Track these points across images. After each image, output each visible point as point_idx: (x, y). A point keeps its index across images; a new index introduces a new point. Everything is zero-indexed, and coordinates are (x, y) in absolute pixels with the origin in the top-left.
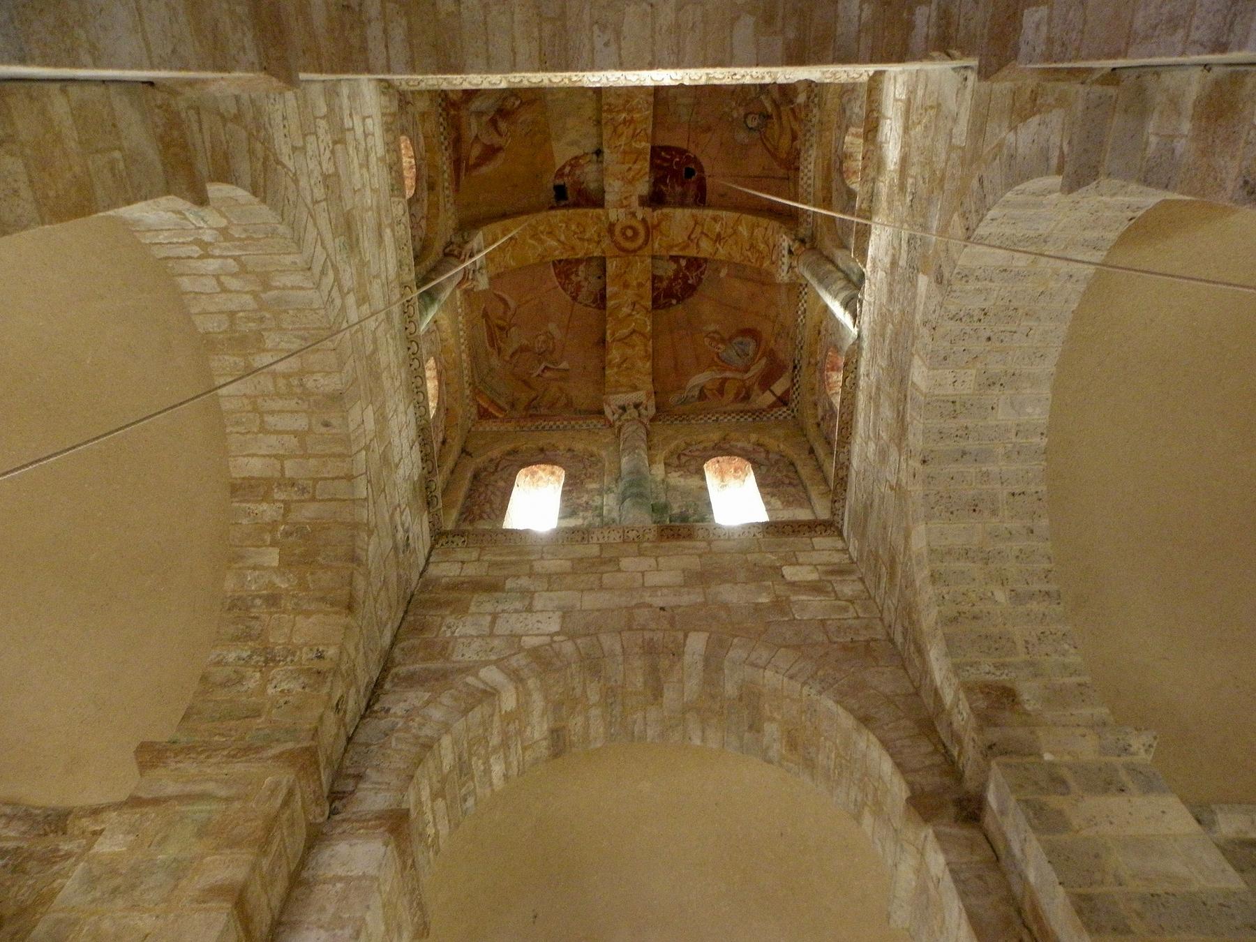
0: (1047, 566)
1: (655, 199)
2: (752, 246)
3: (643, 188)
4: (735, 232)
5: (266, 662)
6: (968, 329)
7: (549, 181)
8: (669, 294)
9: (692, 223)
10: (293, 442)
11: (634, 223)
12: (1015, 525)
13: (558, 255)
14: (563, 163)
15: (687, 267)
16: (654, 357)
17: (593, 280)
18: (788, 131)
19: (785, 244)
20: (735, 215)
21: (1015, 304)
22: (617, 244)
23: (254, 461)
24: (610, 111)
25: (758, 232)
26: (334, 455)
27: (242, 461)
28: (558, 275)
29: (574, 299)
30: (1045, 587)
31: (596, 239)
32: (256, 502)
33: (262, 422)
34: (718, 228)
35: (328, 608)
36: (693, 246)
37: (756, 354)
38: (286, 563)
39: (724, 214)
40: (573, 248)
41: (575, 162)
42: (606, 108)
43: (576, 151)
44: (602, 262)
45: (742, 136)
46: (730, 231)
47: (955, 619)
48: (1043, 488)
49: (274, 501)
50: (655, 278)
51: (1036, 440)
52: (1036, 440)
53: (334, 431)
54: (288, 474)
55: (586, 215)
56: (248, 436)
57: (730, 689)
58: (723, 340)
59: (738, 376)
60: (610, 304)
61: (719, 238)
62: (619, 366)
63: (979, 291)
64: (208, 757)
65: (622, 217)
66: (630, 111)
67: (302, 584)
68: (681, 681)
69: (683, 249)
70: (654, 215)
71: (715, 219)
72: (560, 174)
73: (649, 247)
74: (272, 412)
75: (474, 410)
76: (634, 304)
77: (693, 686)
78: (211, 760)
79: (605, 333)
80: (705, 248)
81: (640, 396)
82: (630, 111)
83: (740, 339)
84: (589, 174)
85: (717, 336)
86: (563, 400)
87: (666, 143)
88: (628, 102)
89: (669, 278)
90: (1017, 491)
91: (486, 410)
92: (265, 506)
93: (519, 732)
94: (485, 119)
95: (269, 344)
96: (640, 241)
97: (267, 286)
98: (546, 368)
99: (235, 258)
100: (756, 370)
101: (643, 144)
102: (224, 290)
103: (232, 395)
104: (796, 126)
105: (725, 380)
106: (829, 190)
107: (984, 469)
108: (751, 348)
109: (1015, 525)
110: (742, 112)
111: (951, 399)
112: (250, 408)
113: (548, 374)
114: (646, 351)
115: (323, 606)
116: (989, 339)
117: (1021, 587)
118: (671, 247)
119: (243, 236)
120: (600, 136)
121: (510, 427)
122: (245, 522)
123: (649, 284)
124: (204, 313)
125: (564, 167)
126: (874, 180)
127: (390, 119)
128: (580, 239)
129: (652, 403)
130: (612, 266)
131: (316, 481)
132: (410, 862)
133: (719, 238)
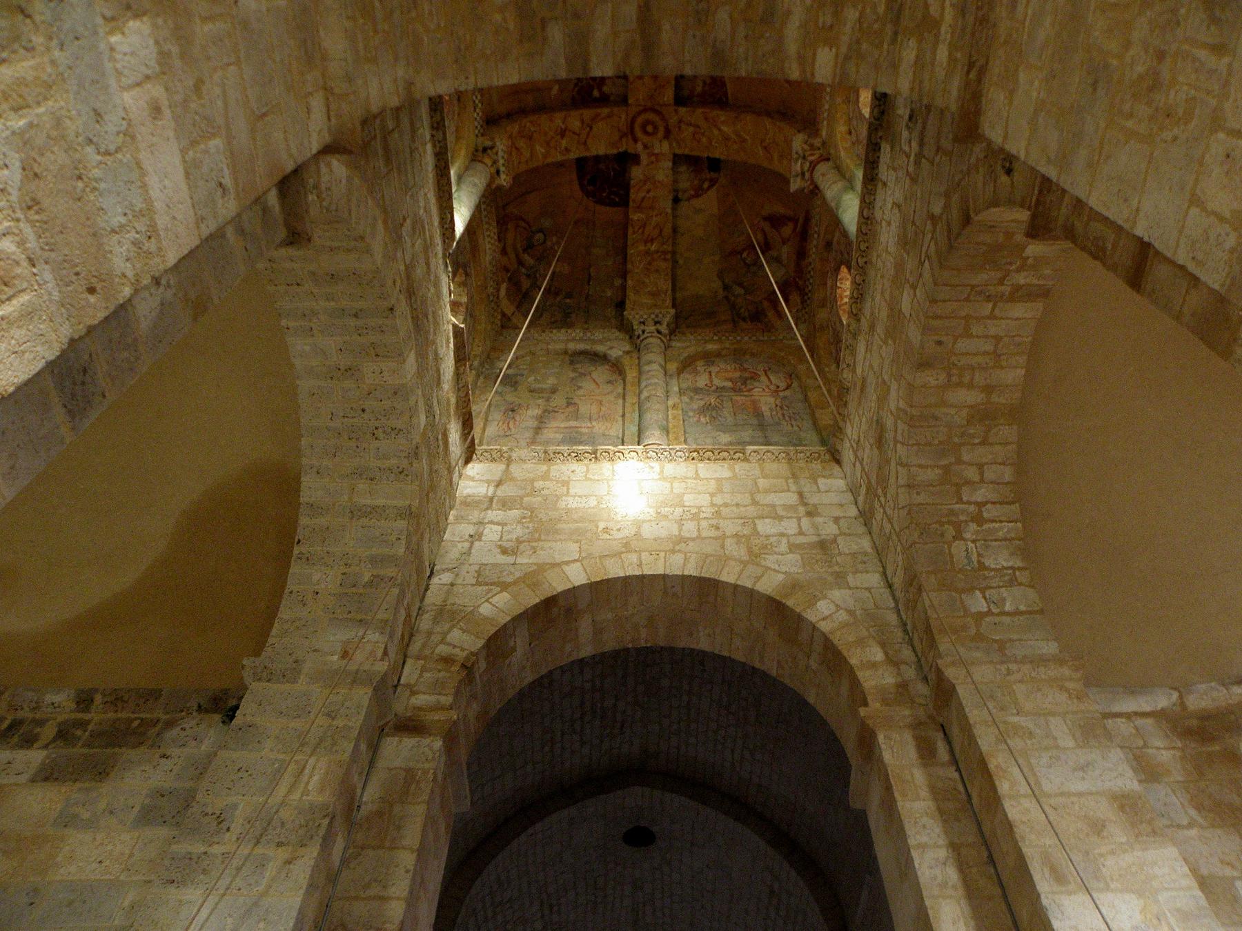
1: (626, 160)
2: (531, 138)
3: (636, 173)
4: (548, 144)
9: (589, 141)
10: (975, 330)
11: (645, 139)
13: (722, 115)
14: (709, 193)
19: (503, 176)
21: (353, 444)
22: (663, 119)
23: (1017, 315)
24: (664, 253)
25: (527, 154)
26: (940, 317)
31: (683, 126)
33: (996, 345)
34: (564, 143)
39: (560, 158)
40: (706, 119)
41: (698, 192)
42: (669, 256)
43: (695, 202)
45: (547, 223)
46: (552, 144)
48: (271, 289)
51: (291, 324)
54: (991, 305)
57: (556, 34)
65: (657, 145)
66: (647, 253)
69: (597, 115)
70: (626, 146)
71: (567, 150)
72: (713, 182)
74: (986, 353)
82: (647, 253)
87: (615, 209)
88: (650, 263)
92: (1022, 282)
95: (964, 412)
96: (640, 120)
97: (946, 469)
99: (960, 501)
102: (980, 466)
103: (1013, 375)
107: (332, 303)
110: (549, 243)
116: (363, 410)
118: (609, 116)
120: (675, 217)
122: (1047, 272)
125: (709, 188)
128: (699, 127)
131: (967, 300)
132: (972, 75)
133: (563, 134)
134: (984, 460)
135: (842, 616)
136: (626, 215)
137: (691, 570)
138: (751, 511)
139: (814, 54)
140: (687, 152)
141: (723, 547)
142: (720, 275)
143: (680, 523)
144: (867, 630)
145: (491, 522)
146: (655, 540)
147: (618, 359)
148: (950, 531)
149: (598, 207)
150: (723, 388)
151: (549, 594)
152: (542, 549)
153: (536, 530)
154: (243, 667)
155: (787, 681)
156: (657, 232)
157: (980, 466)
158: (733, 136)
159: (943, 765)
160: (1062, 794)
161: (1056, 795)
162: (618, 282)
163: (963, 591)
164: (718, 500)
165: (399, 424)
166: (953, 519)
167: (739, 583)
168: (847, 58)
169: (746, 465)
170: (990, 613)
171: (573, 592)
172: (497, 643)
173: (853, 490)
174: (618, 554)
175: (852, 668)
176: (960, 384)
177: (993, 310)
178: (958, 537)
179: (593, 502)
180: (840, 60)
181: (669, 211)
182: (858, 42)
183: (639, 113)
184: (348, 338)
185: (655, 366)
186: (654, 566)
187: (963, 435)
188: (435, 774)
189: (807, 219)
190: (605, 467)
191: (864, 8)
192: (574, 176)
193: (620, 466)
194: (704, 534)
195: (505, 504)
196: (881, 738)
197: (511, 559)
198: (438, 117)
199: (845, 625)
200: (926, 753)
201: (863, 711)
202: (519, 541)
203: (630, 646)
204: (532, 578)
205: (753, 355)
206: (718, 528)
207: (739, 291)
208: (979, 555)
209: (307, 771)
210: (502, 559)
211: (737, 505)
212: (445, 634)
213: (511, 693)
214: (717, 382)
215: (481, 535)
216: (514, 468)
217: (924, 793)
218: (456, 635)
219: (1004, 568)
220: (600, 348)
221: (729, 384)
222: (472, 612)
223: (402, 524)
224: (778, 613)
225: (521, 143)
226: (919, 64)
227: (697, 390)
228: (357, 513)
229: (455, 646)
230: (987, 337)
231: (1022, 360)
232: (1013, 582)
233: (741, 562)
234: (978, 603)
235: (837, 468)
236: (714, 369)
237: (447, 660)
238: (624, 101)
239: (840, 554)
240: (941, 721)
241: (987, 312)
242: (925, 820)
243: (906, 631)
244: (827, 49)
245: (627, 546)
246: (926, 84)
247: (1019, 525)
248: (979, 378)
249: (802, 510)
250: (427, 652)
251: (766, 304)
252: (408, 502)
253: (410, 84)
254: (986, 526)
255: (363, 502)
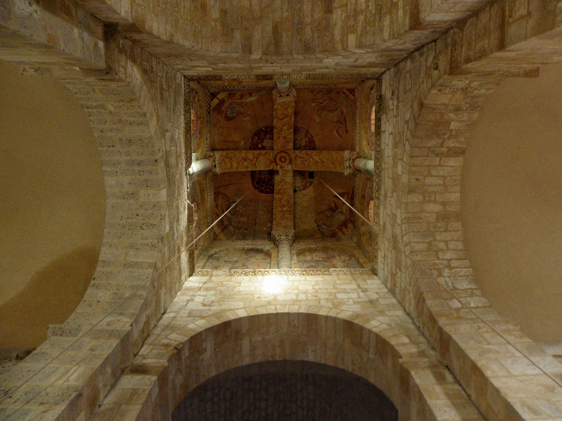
0: (91, 118)
1: (272, 173)
2: (231, 159)
3: (277, 178)
5: (467, 89)
6: (147, 220)
7: (315, 181)
8: (266, 132)
10: (434, 172)
12: (110, 134)
13: (314, 153)
15: (258, 144)
16: (272, 109)
17: (299, 139)
18: (219, 207)
19: (217, 169)
20: (238, 170)
21: (130, 232)
22: (289, 156)
24: (291, 211)
27: (457, 164)
28: (314, 141)
29: (307, 131)
30: (90, 110)
31: (297, 158)
32: (456, 147)
33: (444, 181)
34: (246, 164)
35: (432, 106)
36: (256, 155)
37: (227, 111)
38: (448, 123)
40: (307, 155)
42: (292, 213)
43: (303, 192)
44: (295, 148)
47: (131, 100)
48: (100, 149)
49: (447, 147)
50: (272, 139)
51: (108, 169)
52: (108, 169)
53: (415, 177)
54: (438, 159)
55: (301, 168)
56: (451, 175)
57: (238, 35)
58: (242, 113)
59: (234, 101)
60: (292, 130)
61: (245, 159)
62: (288, 107)
63: (146, 239)
64: (503, 74)
66: (282, 211)
67: (442, 115)
68: (263, 38)
69: (260, 153)
70: (273, 167)
71: (247, 167)
72: (311, 183)
73: (275, 153)
74: (440, 185)
75: (356, 93)
76: (281, 130)
77: (257, 36)
78: (502, 72)
79: (295, 119)
80: (250, 155)
81: (279, 100)
82: (282, 211)
83: (234, 115)
84: (299, 182)
85: (244, 115)
86: (315, 92)
88: (283, 215)
89: (266, 139)
90: (112, 148)
91: (351, 93)
92: (452, 145)
93: (348, 17)
94: (340, 210)
95: (434, 216)
96: (278, 156)
97: (429, 243)
98: (322, 103)
99: (438, 258)
100: (226, 105)
101: (277, 197)
102: (446, 242)
103: (455, 196)
104: (216, 210)
105: (240, 99)
106: (201, 194)
107: (128, 157)
108: (228, 114)
109: (110, 134)
111: (148, 188)
112: (448, 187)
113: (321, 101)
114: (276, 112)
115: (435, 107)
116: (137, 215)
117: (102, 111)
118: (265, 154)
119: (433, 271)
120: (294, 198)
121: (340, 86)
122: (462, 139)
123: (275, 138)
124: (457, 231)
125: (309, 186)
126: (188, 237)
127: (375, 260)
129: (274, 97)
130: (291, 145)
131: (427, 156)
133: (245, 159)
134: (448, 239)
135: (385, 326)
136: (273, 197)
137: (303, 310)
138: (334, 291)
139: (347, 38)
140: (299, 169)
141: (319, 303)
142: (316, 221)
143: (297, 295)
144: (399, 331)
145: (199, 295)
146: (284, 301)
147: (268, 250)
148: (436, 273)
149: (261, 194)
150: (319, 260)
151: (226, 319)
152: (224, 304)
153: (222, 298)
154: (48, 328)
155: (357, 372)
156: (286, 202)
157: (446, 242)
158: (319, 161)
159: (451, 384)
160: (524, 375)
161: (520, 376)
162: (269, 225)
163: (446, 299)
164: (317, 287)
165: (155, 222)
166: (436, 267)
167: (328, 315)
168: (361, 35)
169: (331, 277)
170: (462, 308)
171: (239, 320)
172: (196, 341)
173: (385, 283)
174: (264, 306)
175: (392, 346)
176: (430, 201)
177: (440, 162)
178: (440, 275)
179: (252, 288)
180: (358, 37)
181: (292, 194)
182: (365, 28)
183: (278, 153)
184: (134, 177)
185: (286, 249)
186: (281, 310)
187: (435, 227)
188: (150, 394)
189: (353, 191)
190: (260, 278)
191: (366, 14)
192: (250, 180)
193: (267, 277)
194: (309, 298)
195: (207, 289)
196: (413, 373)
197: (208, 308)
198: (188, 108)
199: (386, 330)
200: (440, 379)
201: (400, 360)
202: (212, 302)
203: (270, 359)
204: (217, 315)
205: (332, 249)
206: (316, 296)
207: (324, 227)
208: (453, 283)
209: (71, 372)
210: (202, 308)
211: (326, 289)
212: (168, 335)
213: (202, 380)
214: (315, 258)
215: (192, 300)
216: (213, 278)
217: (442, 396)
218: (173, 336)
219: (466, 289)
220: (260, 247)
221: (322, 259)
222: (184, 327)
223: (150, 271)
224: (351, 329)
225: (227, 160)
226: (392, 23)
227: (306, 261)
228: (128, 265)
229: (171, 340)
230: (439, 176)
231: (458, 188)
232: (472, 295)
233: (329, 308)
234: (456, 304)
235: (375, 277)
236: (314, 255)
237: (167, 346)
238: (272, 149)
239: (381, 305)
240: (447, 356)
241: (437, 162)
242: (445, 408)
243: (420, 331)
244: (352, 35)
245: (269, 303)
246: (396, 29)
247: (471, 269)
248: (439, 198)
249: (359, 290)
250: (156, 342)
251: (337, 230)
252: (154, 260)
253: (172, 35)
254: (453, 270)
255: (131, 260)
